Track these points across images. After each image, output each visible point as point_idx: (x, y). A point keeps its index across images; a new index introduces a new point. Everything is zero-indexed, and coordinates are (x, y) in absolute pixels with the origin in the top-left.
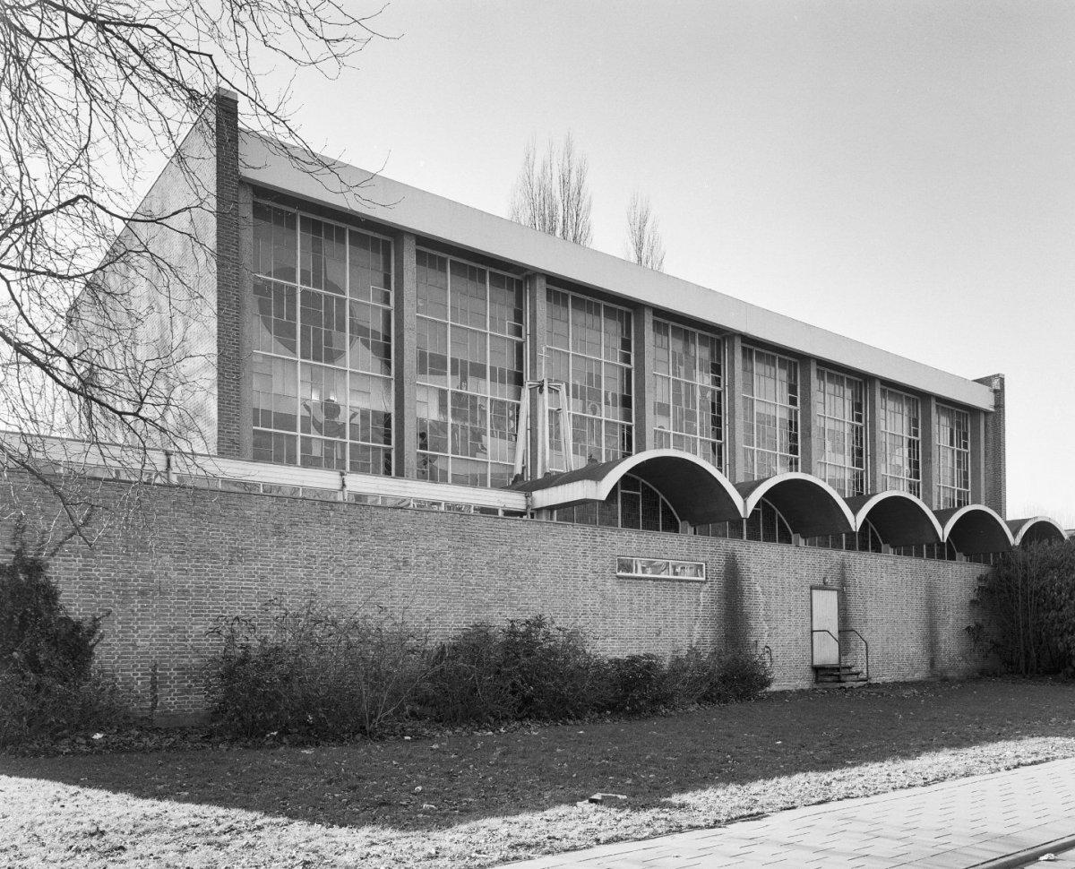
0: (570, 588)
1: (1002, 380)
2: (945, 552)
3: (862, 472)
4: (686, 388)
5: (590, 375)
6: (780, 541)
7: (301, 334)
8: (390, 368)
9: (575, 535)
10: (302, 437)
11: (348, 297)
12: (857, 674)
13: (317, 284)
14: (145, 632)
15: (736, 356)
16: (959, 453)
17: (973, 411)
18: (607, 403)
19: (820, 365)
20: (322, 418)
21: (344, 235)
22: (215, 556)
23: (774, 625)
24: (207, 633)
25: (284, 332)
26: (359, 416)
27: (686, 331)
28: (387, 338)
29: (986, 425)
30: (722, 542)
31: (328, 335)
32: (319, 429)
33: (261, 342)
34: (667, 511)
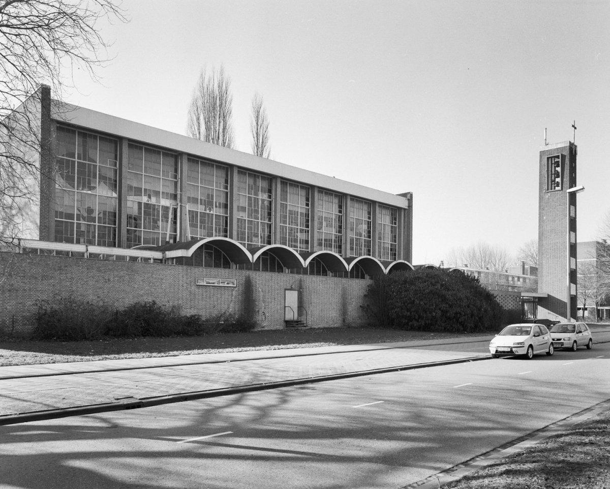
0: (176, 290)
1: (411, 195)
4: (254, 200)
5: (208, 195)
6: (270, 271)
7: (77, 180)
9: (181, 270)
10: (77, 223)
11: (98, 164)
12: (303, 324)
14: (10, 304)
17: (399, 209)
18: (216, 207)
20: (86, 215)
22: (36, 278)
23: (267, 304)
24: (33, 305)
25: (69, 179)
26: (102, 213)
27: (255, 175)
28: (116, 181)
29: (404, 215)
30: (244, 272)
31: (89, 180)
32: (84, 219)
33: (59, 183)
34: (225, 258)
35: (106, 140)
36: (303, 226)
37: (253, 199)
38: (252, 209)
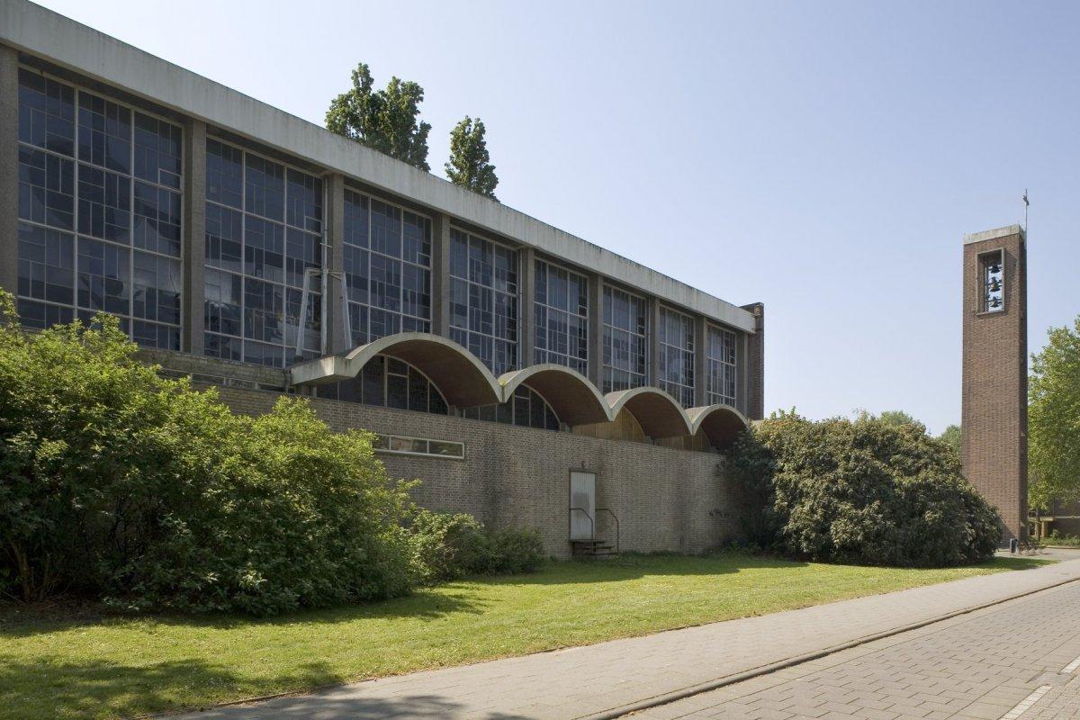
2: (691, 444)
3: (644, 377)
8: (180, 249)
12: (610, 548)
13: (98, 160)
15: (529, 266)
16: (727, 366)
17: (740, 332)
19: (538, 256)
21: (130, 116)
27: (484, 242)
35: (676, 317)
36: (484, 341)
37: (480, 292)
38: (478, 312)
